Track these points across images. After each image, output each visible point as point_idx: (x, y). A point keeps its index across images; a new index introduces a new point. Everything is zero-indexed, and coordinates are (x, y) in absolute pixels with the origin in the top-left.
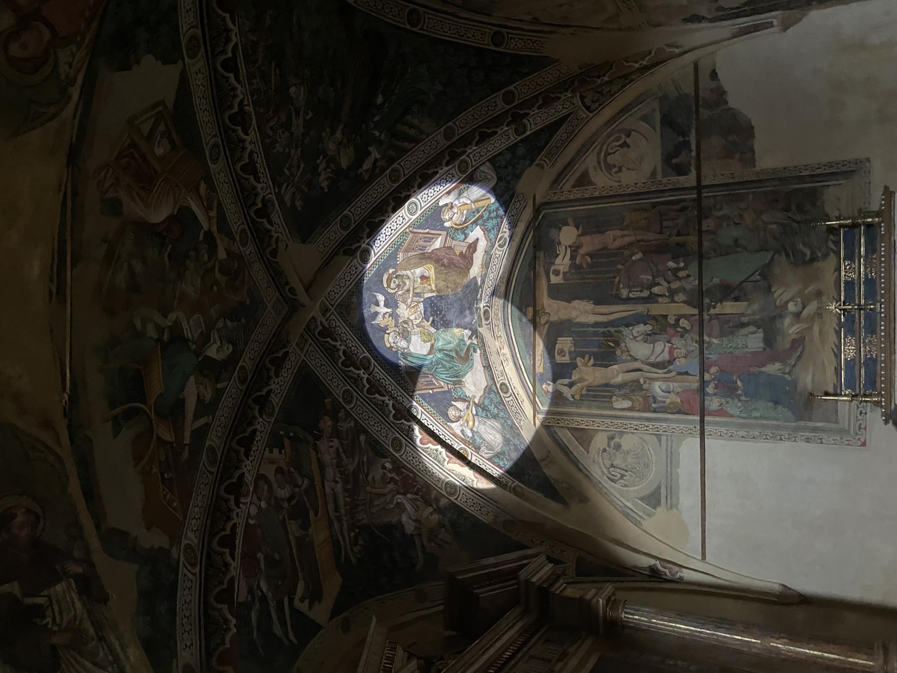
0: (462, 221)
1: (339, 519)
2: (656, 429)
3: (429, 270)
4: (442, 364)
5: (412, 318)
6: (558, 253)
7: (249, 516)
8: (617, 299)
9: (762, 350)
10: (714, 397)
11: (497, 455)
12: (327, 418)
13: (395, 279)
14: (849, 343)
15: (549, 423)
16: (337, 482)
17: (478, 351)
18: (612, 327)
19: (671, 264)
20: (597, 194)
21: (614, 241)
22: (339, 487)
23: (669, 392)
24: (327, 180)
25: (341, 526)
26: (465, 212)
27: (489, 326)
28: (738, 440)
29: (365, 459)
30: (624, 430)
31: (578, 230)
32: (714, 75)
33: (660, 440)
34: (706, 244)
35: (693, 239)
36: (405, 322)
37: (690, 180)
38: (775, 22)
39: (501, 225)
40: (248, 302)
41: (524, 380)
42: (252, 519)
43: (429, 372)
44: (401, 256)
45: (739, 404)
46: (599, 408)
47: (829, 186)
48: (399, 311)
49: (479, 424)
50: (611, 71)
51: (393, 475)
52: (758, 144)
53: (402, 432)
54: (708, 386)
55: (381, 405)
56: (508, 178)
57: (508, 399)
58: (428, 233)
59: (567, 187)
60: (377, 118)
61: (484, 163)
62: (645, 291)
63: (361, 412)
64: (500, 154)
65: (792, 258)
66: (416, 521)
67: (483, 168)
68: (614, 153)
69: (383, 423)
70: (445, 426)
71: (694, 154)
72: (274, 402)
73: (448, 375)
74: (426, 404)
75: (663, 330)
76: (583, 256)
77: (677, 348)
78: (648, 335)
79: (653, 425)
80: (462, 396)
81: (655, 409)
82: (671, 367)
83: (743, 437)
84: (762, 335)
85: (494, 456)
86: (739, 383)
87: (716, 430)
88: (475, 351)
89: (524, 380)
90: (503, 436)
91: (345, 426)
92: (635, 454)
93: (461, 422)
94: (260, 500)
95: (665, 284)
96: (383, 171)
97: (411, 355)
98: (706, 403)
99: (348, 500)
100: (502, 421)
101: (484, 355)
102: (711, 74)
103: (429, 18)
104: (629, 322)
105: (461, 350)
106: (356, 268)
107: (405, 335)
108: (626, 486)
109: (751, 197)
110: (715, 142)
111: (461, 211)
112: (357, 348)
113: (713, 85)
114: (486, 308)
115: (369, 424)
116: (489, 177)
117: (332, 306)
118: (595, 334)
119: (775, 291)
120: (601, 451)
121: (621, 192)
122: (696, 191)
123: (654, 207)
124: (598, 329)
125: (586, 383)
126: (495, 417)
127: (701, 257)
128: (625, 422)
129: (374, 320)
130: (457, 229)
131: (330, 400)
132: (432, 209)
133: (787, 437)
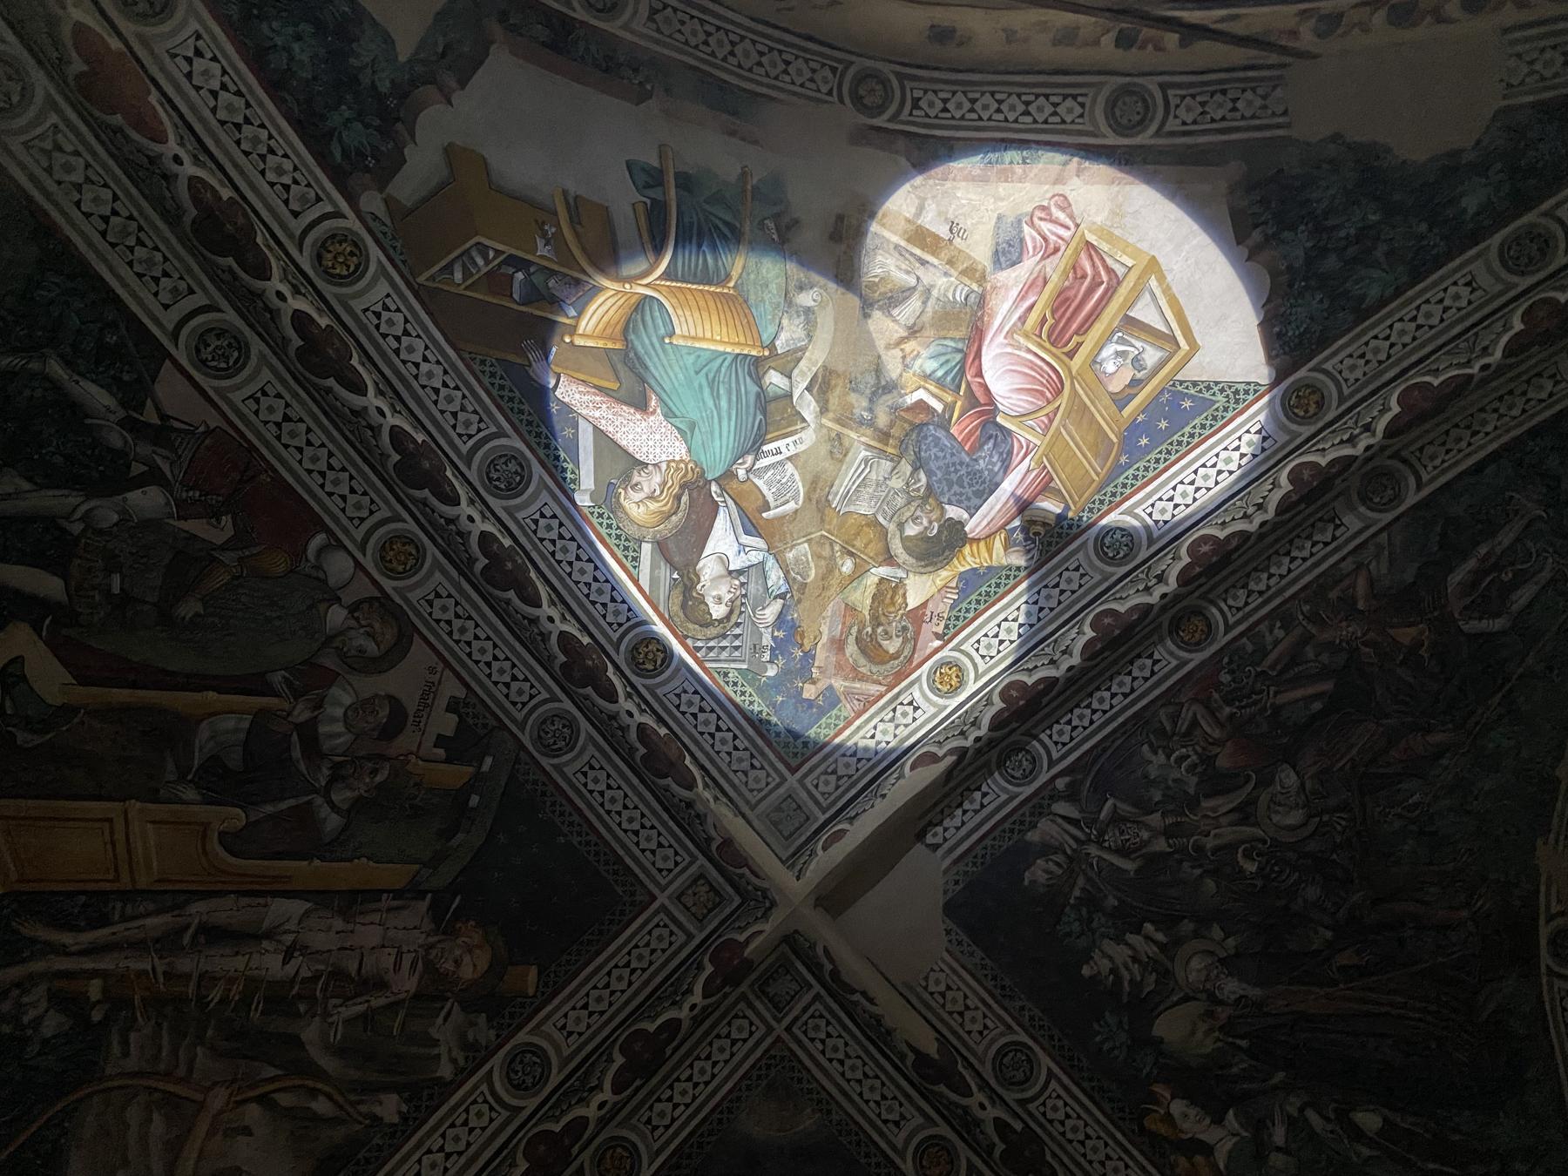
1: (168, 943)
16: (288, 957)
22: (271, 964)
24: (1112, 971)
25: (138, 946)
29: (322, 1106)
40: (809, 692)
94: (353, 609)
99: (215, 995)
106: (897, 1124)
112: (667, 1127)
117: (788, 1029)
131: (531, 991)
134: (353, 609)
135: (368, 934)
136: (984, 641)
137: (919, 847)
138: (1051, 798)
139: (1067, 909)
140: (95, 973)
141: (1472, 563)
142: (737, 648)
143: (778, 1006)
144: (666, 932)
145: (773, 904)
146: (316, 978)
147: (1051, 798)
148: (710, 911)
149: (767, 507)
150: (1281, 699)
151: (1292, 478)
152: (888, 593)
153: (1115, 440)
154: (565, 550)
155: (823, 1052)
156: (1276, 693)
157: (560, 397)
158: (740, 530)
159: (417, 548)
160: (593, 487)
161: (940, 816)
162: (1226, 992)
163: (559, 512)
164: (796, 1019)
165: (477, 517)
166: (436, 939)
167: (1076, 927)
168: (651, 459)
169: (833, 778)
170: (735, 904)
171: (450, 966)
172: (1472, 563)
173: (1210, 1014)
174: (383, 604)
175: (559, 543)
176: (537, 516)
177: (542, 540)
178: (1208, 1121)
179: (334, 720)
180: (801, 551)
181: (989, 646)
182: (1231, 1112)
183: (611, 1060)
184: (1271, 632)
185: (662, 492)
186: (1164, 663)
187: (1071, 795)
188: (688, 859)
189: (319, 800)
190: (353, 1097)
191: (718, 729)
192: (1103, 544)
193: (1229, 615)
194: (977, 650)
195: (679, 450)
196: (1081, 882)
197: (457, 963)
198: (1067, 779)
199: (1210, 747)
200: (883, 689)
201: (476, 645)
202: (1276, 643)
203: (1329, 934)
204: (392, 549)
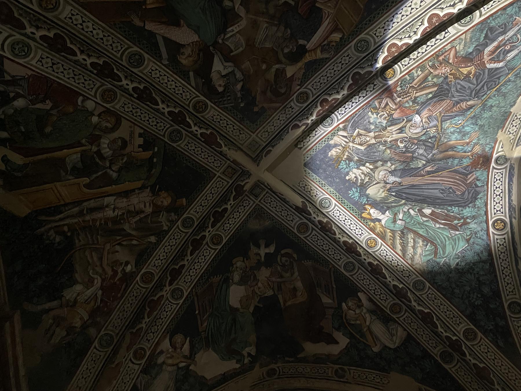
1: (81, 213)
3: (302, 297)
5: (260, 284)
7: (86, 98)
12: (169, 200)
13: (289, 261)
17: (238, 366)
22: (110, 213)
24: (355, 177)
25: (72, 216)
26: (358, 322)
29: (134, 242)
36: (255, 276)
40: (256, 109)
42: (83, 101)
44: (308, 263)
48: (263, 268)
58: (333, 288)
60: (411, 211)
61: (405, 330)
63: (176, 238)
64: (418, 344)
66: (76, 301)
67: (400, 329)
69: (167, 261)
70: (166, 331)
72: (181, 142)
91: (163, 219)
93: (170, 350)
94: (99, 115)
96: (373, 230)
97: (228, 287)
99: (98, 223)
106: (292, 221)
107: (243, 281)
114: (277, 369)
115: (166, 246)
116: (394, 338)
117: (260, 201)
129: (253, 244)
131: (185, 204)
134: (99, 115)
135: (135, 200)
136: (315, 84)
137: (296, 149)
138: (338, 130)
139: (342, 162)
140: (64, 225)
141: (495, 44)
142: (229, 99)
143: (256, 196)
144: (221, 183)
145: (251, 174)
146: (123, 214)
147: (338, 130)
148: (233, 175)
149: (232, 51)
150: (418, 94)
151: (430, 20)
152: (279, 73)
153: (362, 7)
154: (163, 79)
155: (270, 206)
156: (416, 93)
157: (147, 29)
158: (223, 61)
159: (113, 92)
160: (167, 57)
161: (302, 139)
162: (390, 180)
163: (157, 68)
164: (262, 198)
165: (129, 83)
166: (154, 198)
167: (345, 166)
168: (186, 43)
169: (267, 133)
170: (240, 172)
171: (160, 203)
172: (495, 44)
173: (384, 187)
174: (108, 111)
175: (161, 78)
176: (151, 71)
177: (154, 78)
179: (106, 148)
180: (247, 64)
181: (317, 86)
183: (210, 219)
184: (417, 72)
185: (192, 53)
186: (378, 85)
187: (345, 129)
188: (224, 162)
189: (108, 170)
191: (227, 124)
192: (357, 46)
193: (402, 68)
194: (313, 87)
195: (196, 38)
196: (347, 154)
197: (162, 202)
198: (343, 125)
199: (391, 111)
200: (281, 104)
201: (142, 116)
202: (418, 76)
203: (424, 162)
204: (105, 95)
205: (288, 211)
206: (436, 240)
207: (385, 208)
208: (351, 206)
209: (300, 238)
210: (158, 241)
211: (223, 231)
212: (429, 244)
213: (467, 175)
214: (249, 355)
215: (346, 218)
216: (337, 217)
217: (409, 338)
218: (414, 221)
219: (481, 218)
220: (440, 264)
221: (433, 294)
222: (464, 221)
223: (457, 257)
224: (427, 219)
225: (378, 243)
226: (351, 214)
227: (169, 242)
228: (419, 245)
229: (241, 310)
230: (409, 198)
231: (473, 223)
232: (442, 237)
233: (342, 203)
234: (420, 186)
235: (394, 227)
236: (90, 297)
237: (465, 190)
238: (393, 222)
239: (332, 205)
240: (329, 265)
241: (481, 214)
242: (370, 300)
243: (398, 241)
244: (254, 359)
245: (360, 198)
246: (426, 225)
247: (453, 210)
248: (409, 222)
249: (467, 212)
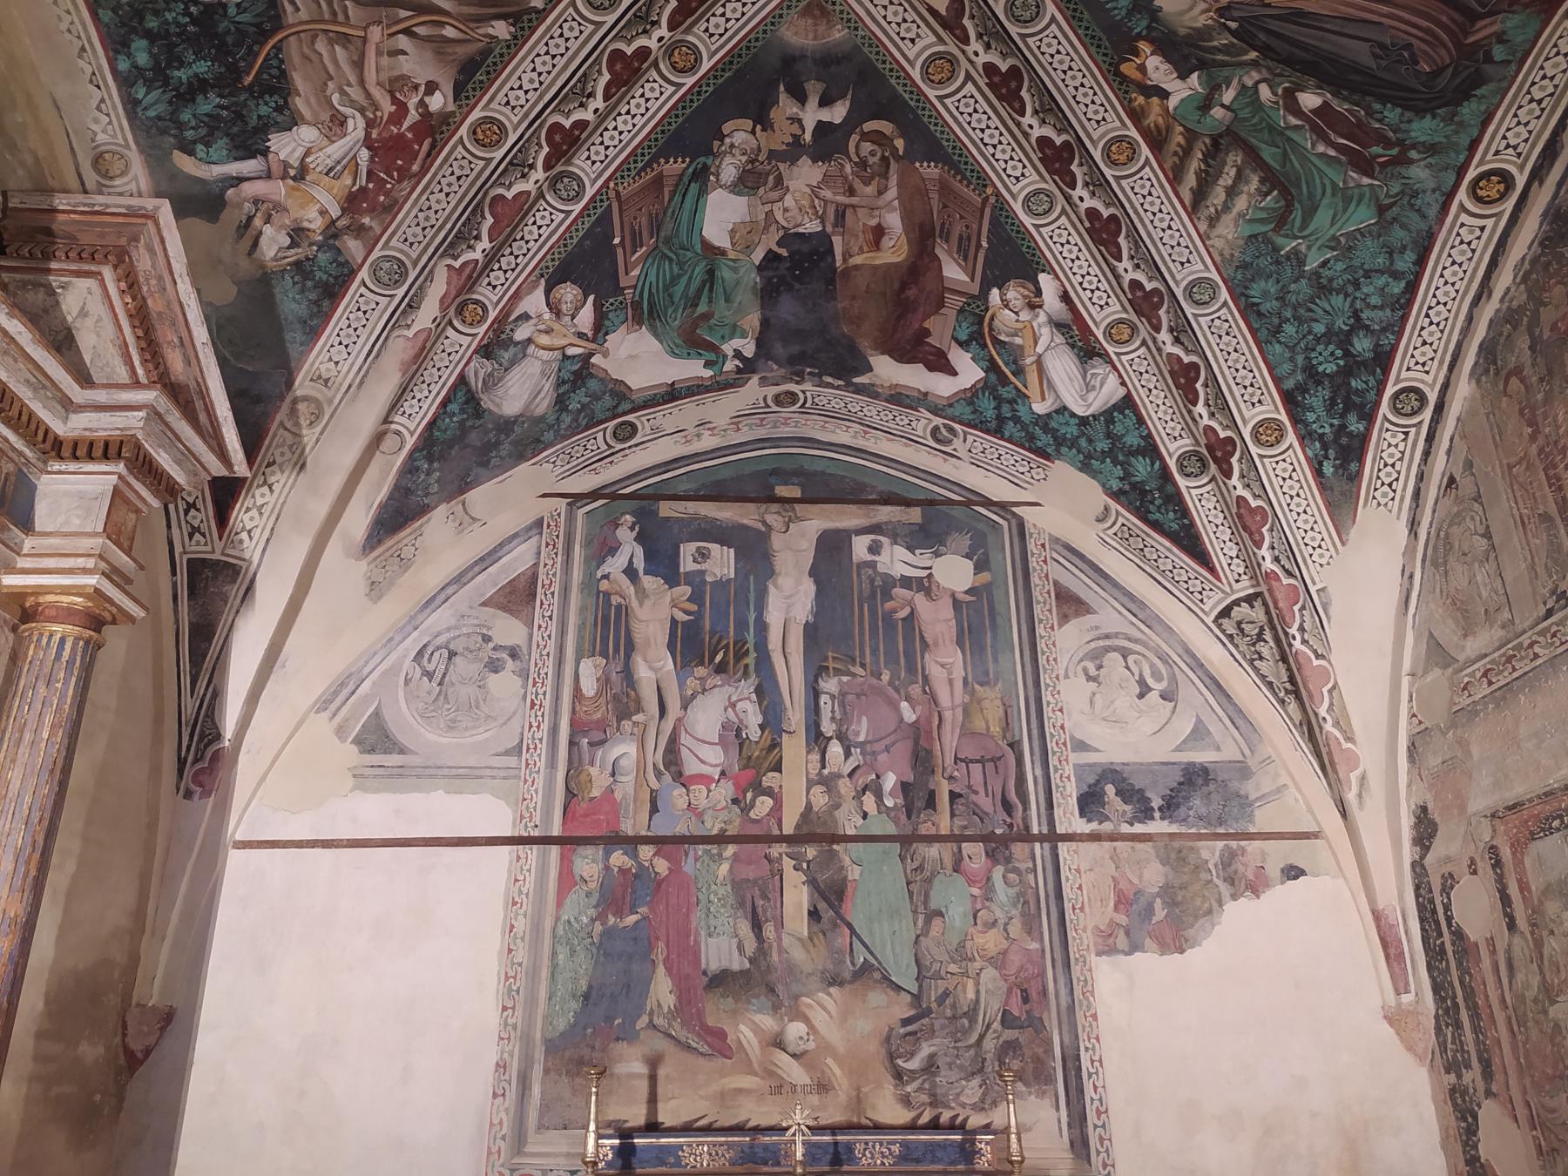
0: (999, 333)
2: (532, 746)
4: (680, 276)
5: (789, 201)
6: (918, 552)
8: (816, 672)
9: (703, 966)
10: (601, 865)
11: (472, 400)
13: (879, 155)
14: (717, 1154)
15: (549, 526)
17: (708, 373)
18: (757, 658)
19: (890, 781)
20: (1040, 630)
21: (943, 666)
23: (613, 774)
26: (1018, 341)
27: (763, 404)
28: (505, 917)
29: (449, 32)
30: (531, 680)
31: (966, 592)
32: (1293, 873)
33: (507, 753)
34: (934, 851)
35: (944, 822)
36: (779, 181)
37: (1069, 819)
38: (1407, 999)
39: (981, 431)
41: (643, 477)
43: (661, 240)
44: (931, 171)
45: (585, 920)
46: (581, 628)
47: (1058, 1109)
48: (805, 161)
49: (544, 362)
50: (1313, 657)
51: (413, 112)
52: (1148, 962)
53: (520, 151)
54: (626, 853)
55: (583, 90)
56: (1083, 443)
57: (600, 436)
58: (979, 246)
59: (1056, 572)
60: (1265, 92)
61: (1123, 384)
62: (834, 727)
64: (1141, 421)
65: (902, 1031)
67: (1113, 379)
68: (1127, 668)
69: (540, 97)
71: (1125, 829)
73: (654, 290)
74: (587, 226)
75: (748, 763)
76: (911, 603)
77: (709, 791)
78: (739, 731)
79: (541, 740)
80: (606, 323)
81: (578, 744)
82: (667, 778)
83: (512, 927)
84: (736, 967)
85: (469, 391)
86: (633, 919)
87: (529, 871)
88: (708, 365)
89: (643, 477)
90: (517, 417)
92: (477, 702)
95: (847, 769)
96: (1136, 116)
97: (703, 192)
98: (589, 851)
100: (551, 419)
101: (699, 386)
102: (1296, 867)
103: (1482, 229)
104: (767, 694)
105: (710, 328)
106: (913, 41)
107: (748, 182)
108: (407, 682)
109: (1034, 946)
110: (1153, 875)
111: (1021, 330)
112: (721, 35)
113: (1273, 871)
114: (801, 396)
116: (1092, 396)
118: (742, 625)
119: (829, 994)
120: (485, 632)
121: (1045, 679)
122: (1045, 831)
123: (1011, 745)
124: (752, 630)
125: (635, 603)
126: (560, 402)
127: (906, 841)
128: (549, 682)
129: (788, 90)
130: (981, 323)
132: (1034, 255)
133: (510, 1021)
178: (1175, 75)
182: (1196, 74)
190: (471, 25)
205: (905, 10)
206: (1299, 187)
207: (1194, 61)
208: (1099, 33)
209: (926, 96)
210: (515, 38)
211: (705, 36)
212: (1275, 193)
213: (1474, 17)
214: (738, 354)
215: (1073, 64)
216: (1047, 56)
217: (1128, 403)
218: (1262, 120)
219: (1453, 155)
220: (1279, 251)
221: (1227, 321)
222: (1400, 152)
223: (1333, 244)
224: (1300, 123)
225: (1140, 155)
226: (1090, 56)
227: (547, 44)
228: (1246, 189)
229: (732, 255)
230: (1272, 50)
231: (1423, 163)
232: (1318, 181)
233: (1074, 17)
234: (1321, 21)
235: (1199, 122)
236: (339, 162)
237: (1448, 61)
238: (1199, 108)
239: (1044, 15)
240: (985, 186)
241: (1457, 144)
242: (1065, 297)
243: (1194, 165)
244: (748, 367)
245: (1130, 12)
246: (1289, 139)
247: (1386, 113)
248: (1245, 119)
249: (1423, 129)
